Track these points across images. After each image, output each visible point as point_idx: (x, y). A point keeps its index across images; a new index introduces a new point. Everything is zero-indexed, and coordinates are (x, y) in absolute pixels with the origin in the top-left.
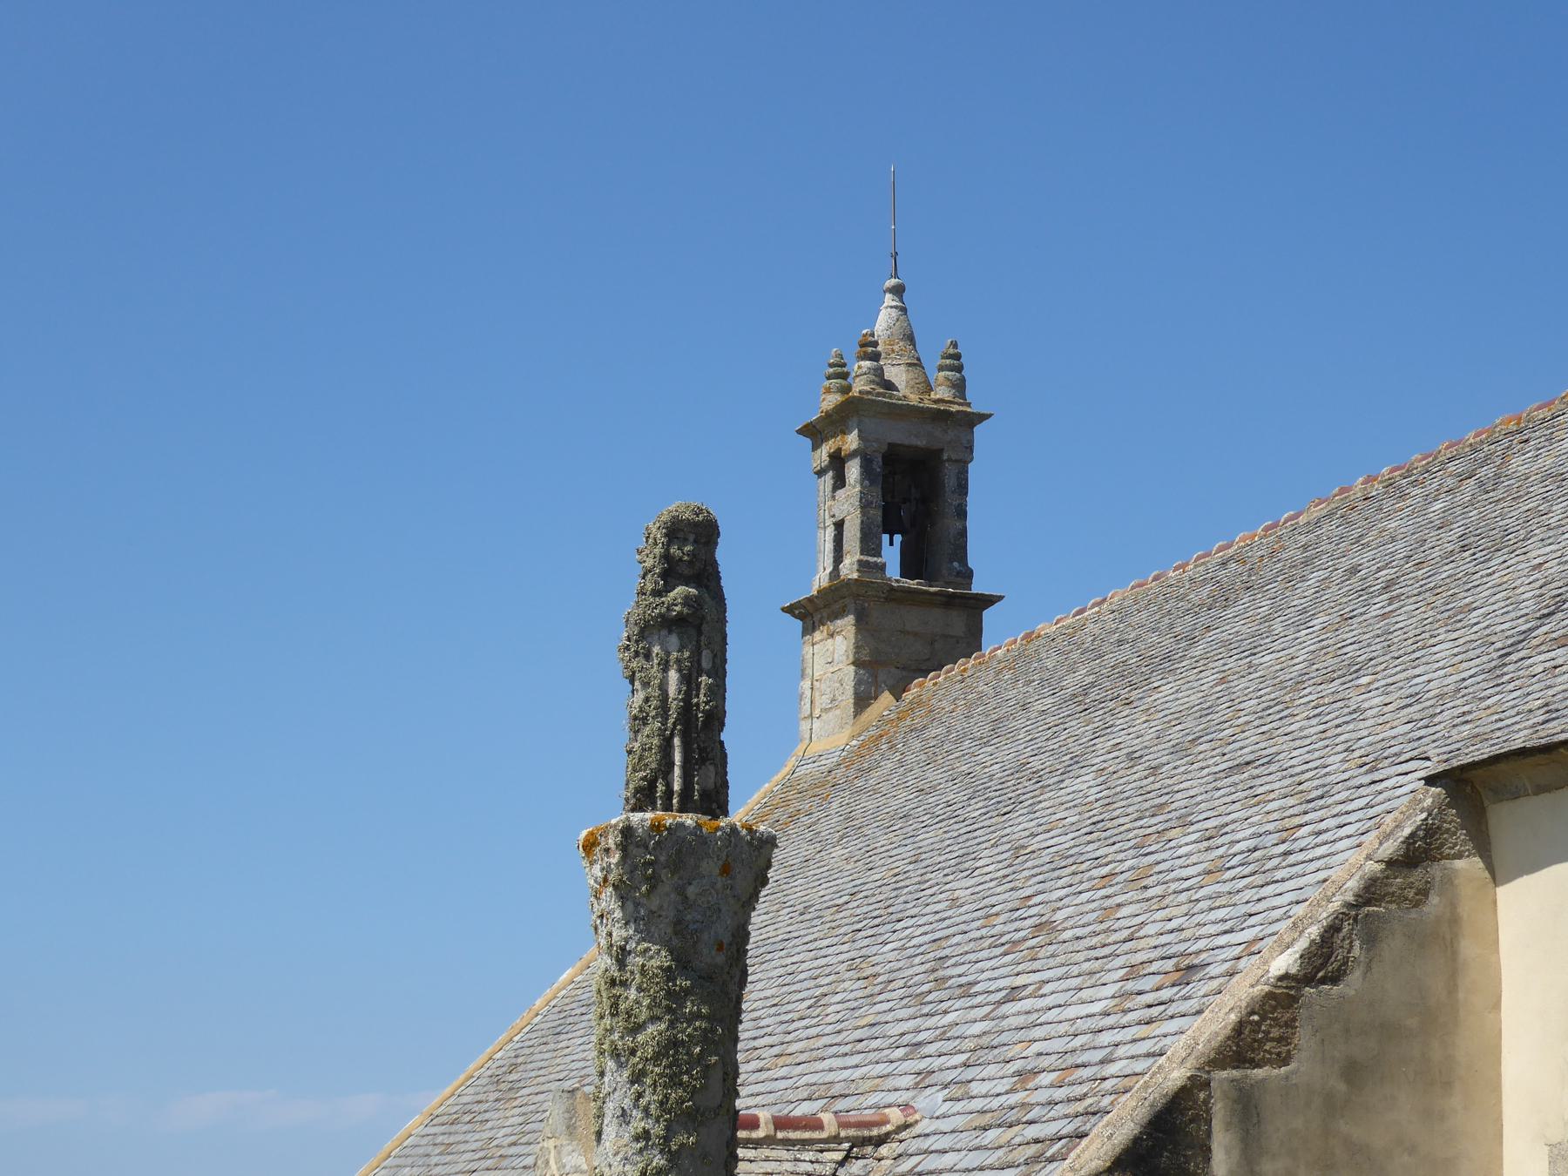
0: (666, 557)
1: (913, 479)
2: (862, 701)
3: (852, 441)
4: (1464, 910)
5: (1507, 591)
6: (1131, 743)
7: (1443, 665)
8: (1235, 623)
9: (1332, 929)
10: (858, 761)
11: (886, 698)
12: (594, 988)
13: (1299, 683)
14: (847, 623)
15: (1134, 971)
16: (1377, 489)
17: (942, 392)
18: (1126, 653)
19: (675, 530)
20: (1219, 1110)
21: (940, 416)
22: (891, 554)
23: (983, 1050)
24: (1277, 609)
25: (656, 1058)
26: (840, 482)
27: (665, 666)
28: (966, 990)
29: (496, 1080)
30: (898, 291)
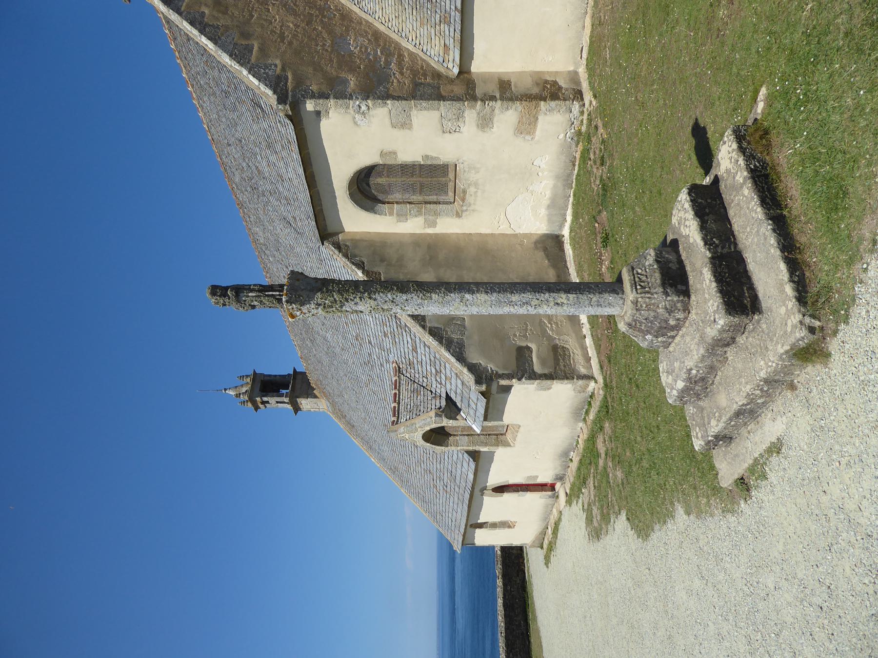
0: (220, 296)
1: (267, 386)
2: (316, 397)
3: (258, 399)
4: (349, 238)
5: (286, 236)
9: (353, 263)
10: (328, 396)
12: (326, 314)
14: (299, 400)
17: (248, 380)
18: (303, 332)
19: (213, 293)
21: (254, 380)
22: (284, 391)
23: (382, 348)
25: (342, 295)
28: (370, 355)
30: (225, 390)
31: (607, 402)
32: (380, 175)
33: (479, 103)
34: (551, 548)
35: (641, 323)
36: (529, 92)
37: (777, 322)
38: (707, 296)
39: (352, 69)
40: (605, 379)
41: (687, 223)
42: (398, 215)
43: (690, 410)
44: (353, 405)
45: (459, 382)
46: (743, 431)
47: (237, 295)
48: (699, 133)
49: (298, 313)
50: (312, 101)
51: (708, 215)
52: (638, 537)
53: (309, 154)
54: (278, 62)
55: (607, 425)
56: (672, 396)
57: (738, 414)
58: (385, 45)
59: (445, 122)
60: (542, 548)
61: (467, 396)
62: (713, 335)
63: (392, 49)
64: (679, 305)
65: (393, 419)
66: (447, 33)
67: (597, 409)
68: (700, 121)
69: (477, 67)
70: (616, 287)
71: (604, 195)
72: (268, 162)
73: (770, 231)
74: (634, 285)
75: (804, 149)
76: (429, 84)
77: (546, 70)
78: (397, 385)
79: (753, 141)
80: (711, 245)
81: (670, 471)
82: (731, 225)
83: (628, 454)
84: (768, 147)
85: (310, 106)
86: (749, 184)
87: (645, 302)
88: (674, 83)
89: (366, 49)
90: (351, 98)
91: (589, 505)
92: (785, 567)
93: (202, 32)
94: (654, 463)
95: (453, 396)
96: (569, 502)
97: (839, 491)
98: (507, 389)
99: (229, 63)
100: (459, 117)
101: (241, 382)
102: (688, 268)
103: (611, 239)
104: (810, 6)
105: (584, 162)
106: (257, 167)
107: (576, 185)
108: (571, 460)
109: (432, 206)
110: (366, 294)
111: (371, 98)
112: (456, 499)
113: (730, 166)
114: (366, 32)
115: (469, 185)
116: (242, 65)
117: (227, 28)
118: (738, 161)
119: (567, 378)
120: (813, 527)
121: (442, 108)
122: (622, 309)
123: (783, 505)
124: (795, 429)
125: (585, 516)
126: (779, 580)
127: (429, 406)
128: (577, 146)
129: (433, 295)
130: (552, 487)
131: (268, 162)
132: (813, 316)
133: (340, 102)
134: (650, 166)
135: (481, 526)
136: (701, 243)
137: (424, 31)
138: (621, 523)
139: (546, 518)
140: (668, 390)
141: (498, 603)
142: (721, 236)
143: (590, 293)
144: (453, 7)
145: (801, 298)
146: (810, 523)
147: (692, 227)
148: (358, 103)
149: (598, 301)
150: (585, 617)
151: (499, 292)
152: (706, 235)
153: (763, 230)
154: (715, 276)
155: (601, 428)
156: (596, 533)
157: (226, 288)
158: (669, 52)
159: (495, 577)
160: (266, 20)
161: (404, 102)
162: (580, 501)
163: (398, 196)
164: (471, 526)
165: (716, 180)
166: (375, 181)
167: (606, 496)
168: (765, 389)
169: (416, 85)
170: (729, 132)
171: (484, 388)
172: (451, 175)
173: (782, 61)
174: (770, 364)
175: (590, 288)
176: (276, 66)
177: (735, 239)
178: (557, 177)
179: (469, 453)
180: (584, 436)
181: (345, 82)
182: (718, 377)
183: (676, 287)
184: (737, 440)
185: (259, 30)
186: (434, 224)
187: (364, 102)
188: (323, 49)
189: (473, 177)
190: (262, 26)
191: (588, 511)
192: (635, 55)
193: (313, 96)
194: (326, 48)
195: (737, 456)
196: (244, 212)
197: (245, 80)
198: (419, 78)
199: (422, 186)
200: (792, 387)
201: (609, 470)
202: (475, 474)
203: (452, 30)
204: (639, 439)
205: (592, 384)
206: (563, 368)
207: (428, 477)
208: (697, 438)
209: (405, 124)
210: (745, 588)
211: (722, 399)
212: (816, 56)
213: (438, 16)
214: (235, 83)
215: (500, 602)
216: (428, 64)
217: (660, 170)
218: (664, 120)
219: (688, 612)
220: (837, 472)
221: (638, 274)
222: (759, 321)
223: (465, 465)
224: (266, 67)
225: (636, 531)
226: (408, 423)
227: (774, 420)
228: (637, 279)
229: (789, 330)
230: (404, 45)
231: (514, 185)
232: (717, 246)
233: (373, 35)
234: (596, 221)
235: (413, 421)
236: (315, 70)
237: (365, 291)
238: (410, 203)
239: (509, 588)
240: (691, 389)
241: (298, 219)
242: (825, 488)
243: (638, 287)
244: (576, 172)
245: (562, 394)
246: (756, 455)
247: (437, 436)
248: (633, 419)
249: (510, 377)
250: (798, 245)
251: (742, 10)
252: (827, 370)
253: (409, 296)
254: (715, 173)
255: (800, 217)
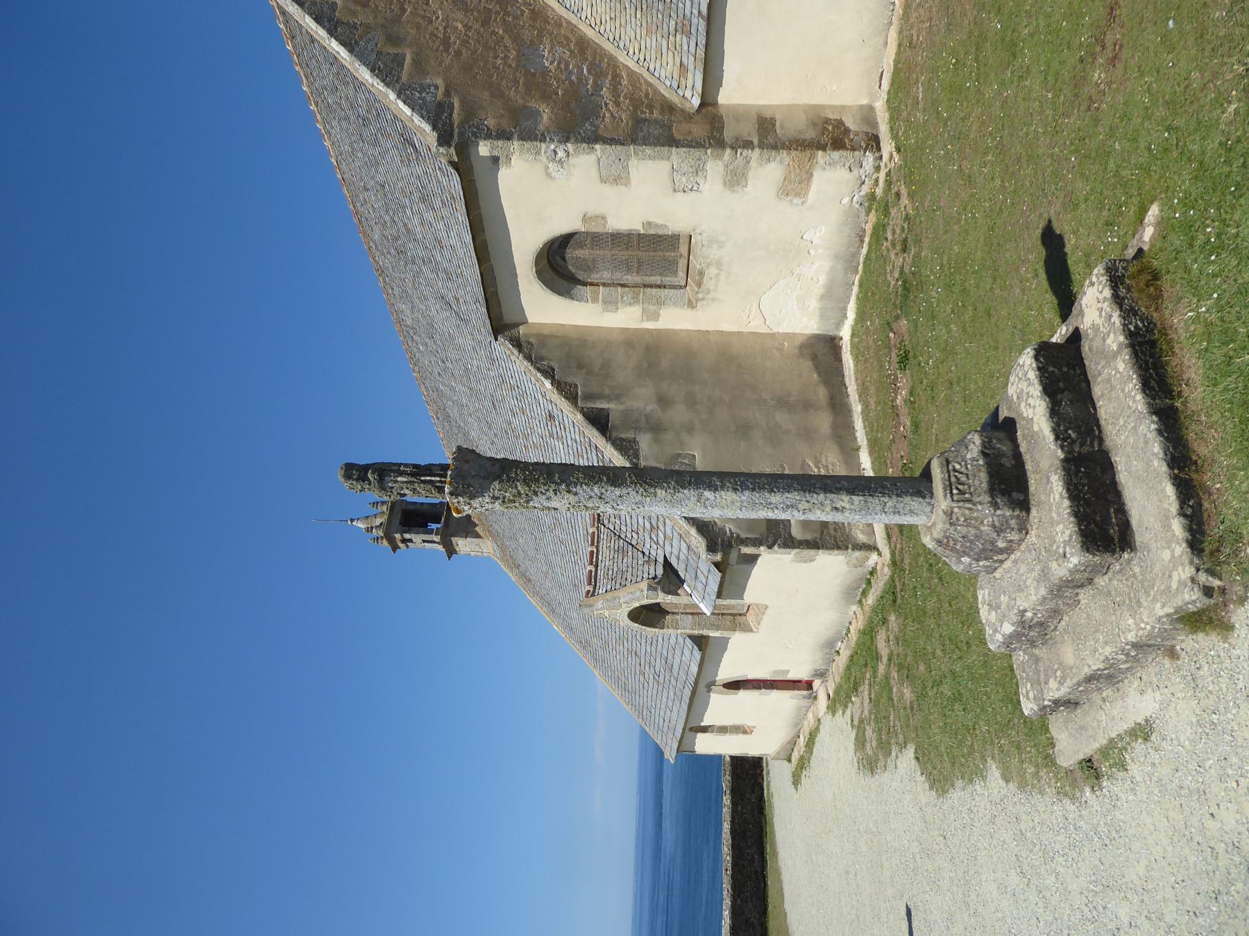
0: (357, 480)
2: (478, 536)
3: (398, 536)
4: (534, 332)
5: (444, 321)
6: (488, 445)
7: (465, 341)
8: (454, 412)
9: (539, 370)
10: (495, 537)
11: (477, 529)
13: (471, 389)
14: (454, 540)
15: (551, 435)
16: (416, 369)
17: (385, 508)
19: (348, 476)
20: (589, 405)
21: (392, 509)
22: (434, 526)
24: (450, 399)
25: (530, 486)
26: (410, 541)
27: (396, 482)
29: (584, 648)
30: (352, 520)
31: (895, 587)
32: (581, 246)
33: (728, 151)
34: (803, 764)
35: (955, 541)
36: (802, 137)
37: (1157, 568)
38: (1054, 515)
39: (546, 96)
40: (893, 554)
41: (1031, 401)
42: (605, 302)
43: (1020, 657)
44: (531, 553)
45: (684, 546)
46: (1096, 697)
47: (381, 480)
48: (1052, 241)
49: (466, 508)
50: (488, 143)
51: (1062, 392)
52: (931, 788)
53: (480, 214)
54: (439, 82)
55: (892, 618)
56: (995, 642)
57: (1089, 679)
58: (594, 59)
59: (677, 177)
60: (790, 761)
61: (695, 565)
62: (1061, 574)
63: (604, 65)
64: (1013, 523)
65: (588, 588)
66: (685, 47)
67: (879, 593)
68: (1055, 225)
69: (726, 97)
70: (919, 485)
71: (905, 297)
72: (422, 219)
73: (1154, 434)
74: (949, 487)
75: (1213, 317)
76: (656, 122)
77: (827, 103)
78: (595, 540)
79: (1134, 283)
80: (1064, 440)
81: (982, 710)
82: (1095, 409)
83: (922, 668)
84: (1157, 297)
85: (484, 149)
86: (1126, 355)
87: (963, 515)
88: (1019, 159)
89: (567, 64)
90: (543, 139)
91: (861, 721)
92: (1146, 900)
93: (331, 33)
94: (960, 694)
95: (674, 562)
96: (832, 709)
97: (1233, 822)
98: (753, 559)
99: (370, 81)
100: (699, 170)
101: (374, 511)
102: (1029, 467)
103: (912, 361)
104: (1233, 107)
105: (877, 241)
106: (405, 225)
107: (864, 271)
108: (838, 652)
109: (654, 291)
110: (563, 486)
111: (572, 140)
112: (671, 694)
113: (1099, 321)
114: (567, 39)
115: (709, 265)
116: (388, 85)
117: (368, 27)
118: (1111, 316)
119: (839, 548)
120: (1192, 859)
121: (674, 157)
122: (930, 518)
123: (1148, 813)
124: (1173, 713)
125: (853, 735)
126: (1136, 914)
127: (640, 573)
128: (868, 214)
129: (659, 491)
130: (809, 685)
131: (422, 219)
132: (1211, 572)
133: (527, 145)
134: (977, 272)
135: (705, 730)
136: (1049, 436)
137: (651, 42)
138: (906, 760)
139: (798, 724)
140: (989, 631)
141: (725, 829)
142: (1079, 427)
143: (883, 494)
144: (695, 12)
145: (1196, 542)
146: (1187, 851)
147: (1037, 409)
148: (552, 147)
149: (895, 507)
150: (848, 873)
151: (753, 490)
152: (1058, 425)
153: (1143, 429)
154: (1068, 490)
155: (885, 621)
156: (870, 765)
157: (366, 468)
158: (1013, 112)
159: (720, 793)
160: (423, 17)
161: (619, 148)
162: (848, 712)
163: (606, 275)
164: (691, 729)
165: (1076, 337)
166: (572, 253)
167: (887, 718)
168: (1133, 654)
169: (638, 122)
170: (1099, 270)
171: (718, 557)
172: (683, 249)
173: (1186, 175)
174: (1143, 625)
175: (884, 487)
176: (436, 87)
177: (1100, 431)
178: (837, 257)
179: (691, 637)
180: (858, 624)
181: (536, 114)
182: (1063, 623)
183: (1010, 496)
184: (1086, 707)
185: (413, 32)
186: (655, 317)
187: (562, 147)
188: (505, 64)
189: (714, 253)
190: (418, 26)
191: (860, 728)
192: (961, 105)
193: (488, 136)
194: (509, 61)
195: (1083, 728)
196: (385, 281)
197: (392, 107)
198: (642, 112)
199: (640, 264)
200: (1172, 654)
201: (892, 682)
202: (701, 666)
203: (693, 44)
204: (939, 652)
205: (874, 558)
206: (832, 532)
207: (632, 660)
208: (1028, 698)
209: (620, 179)
210: (1086, 910)
211: (1068, 654)
212: (1238, 186)
213: (673, 23)
214: (380, 109)
215: (726, 827)
216: (656, 91)
217: (990, 280)
218: (1001, 210)
219: (999, 915)
220: (1232, 794)
221: (955, 470)
222: (1129, 561)
223: (687, 652)
224: (423, 89)
225: (928, 779)
226: (609, 596)
227: (1142, 692)
228: (953, 479)
229: (1174, 585)
230: (621, 59)
231: (773, 264)
232: (1074, 442)
233: (577, 44)
234: (892, 330)
235: (616, 594)
236: (492, 95)
237: (562, 481)
238: (622, 286)
239: (740, 808)
240: (1023, 635)
241: (461, 300)
242: (1214, 810)
243: (955, 491)
244: (865, 250)
245: (832, 567)
246: (1113, 735)
247: (649, 615)
248: (931, 623)
249: (757, 543)
250: (1194, 458)
251: (1128, 79)
252: (1226, 645)
253: (624, 491)
254: (1075, 324)
255: (1199, 416)
